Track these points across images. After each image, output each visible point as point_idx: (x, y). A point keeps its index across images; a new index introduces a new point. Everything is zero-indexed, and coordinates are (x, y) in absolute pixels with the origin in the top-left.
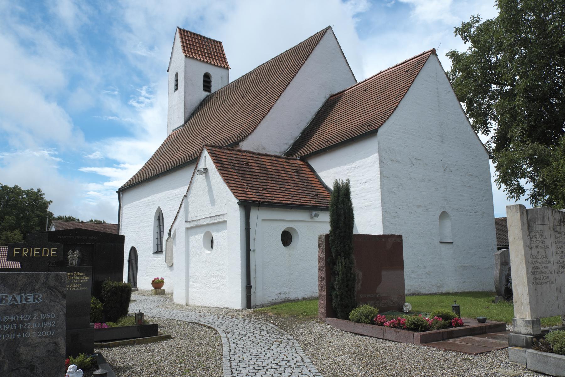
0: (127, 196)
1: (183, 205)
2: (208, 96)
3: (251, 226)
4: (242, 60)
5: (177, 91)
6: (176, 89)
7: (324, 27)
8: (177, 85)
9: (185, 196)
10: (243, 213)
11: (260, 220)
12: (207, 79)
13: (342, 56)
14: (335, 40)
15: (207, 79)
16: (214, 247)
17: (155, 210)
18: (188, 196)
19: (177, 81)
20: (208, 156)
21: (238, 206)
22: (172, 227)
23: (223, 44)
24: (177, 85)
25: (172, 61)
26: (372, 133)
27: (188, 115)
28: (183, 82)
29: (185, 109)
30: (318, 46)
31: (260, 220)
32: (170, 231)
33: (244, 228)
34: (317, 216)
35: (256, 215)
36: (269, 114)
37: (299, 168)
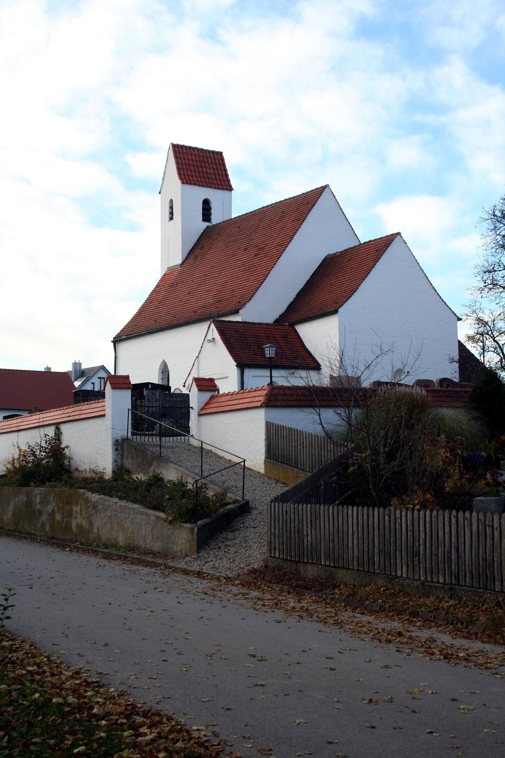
1: (196, 364)
2: (207, 227)
3: (245, 380)
4: (245, 198)
6: (171, 219)
7: (323, 185)
8: (172, 213)
9: (197, 357)
10: (240, 372)
11: (251, 376)
12: (206, 205)
13: (341, 212)
15: (206, 205)
16: (13, 604)
18: (200, 357)
19: (171, 208)
20: (215, 329)
21: (236, 368)
22: (186, 381)
24: (172, 213)
25: (165, 183)
26: (335, 312)
27: (186, 254)
28: (180, 213)
29: (183, 246)
30: (314, 207)
31: (251, 376)
32: (184, 384)
33: (240, 381)
35: (247, 372)
36: (265, 282)
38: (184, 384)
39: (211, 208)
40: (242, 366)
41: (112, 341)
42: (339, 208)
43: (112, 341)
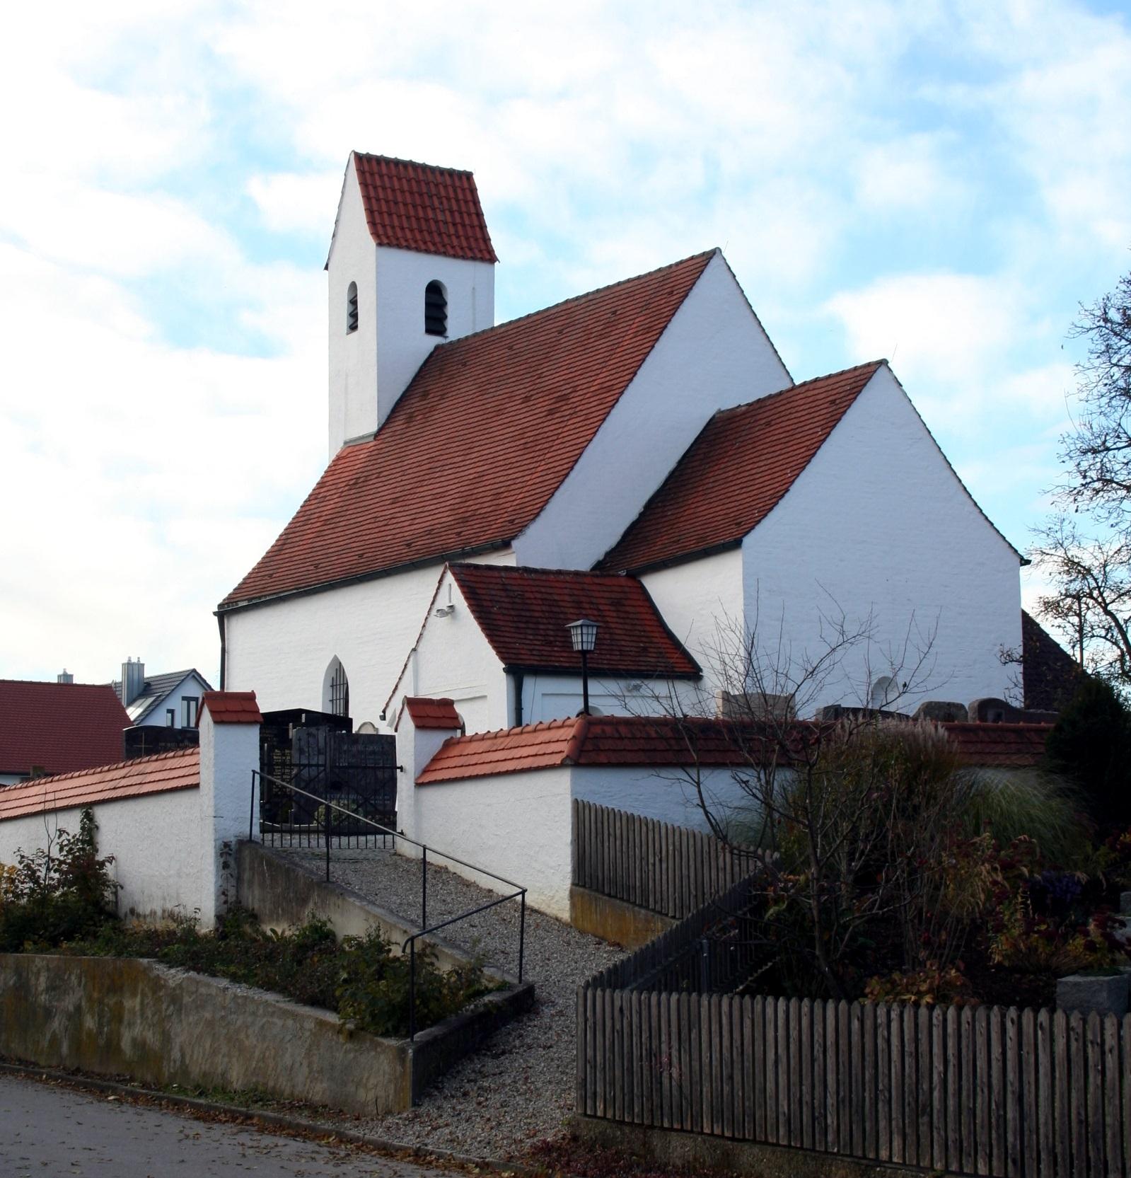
0: (241, 626)
1: (410, 666)
2: (437, 348)
3: (525, 704)
4: (525, 279)
5: (355, 334)
6: (353, 327)
8: (354, 315)
9: (414, 650)
10: (512, 685)
12: (435, 296)
13: (748, 311)
14: (730, 277)
15: (435, 296)
17: (327, 664)
18: (419, 649)
19: (354, 302)
20: (455, 585)
22: (387, 705)
23: (476, 178)
24: (354, 315)
25: (337, 244)
26: (736, 545)
27: (387, 410)
30: (687, 301)
32: (384, 712)
33: (513, 707)
34: (637, 688)
35: (535, 688)
36: (573, 474)
37: (622, 595)
38: (384, 712)
39: (445, 303)
40: (517, 671)
41: (215, 614)
42: (743, 302)
43: (215, 614)
